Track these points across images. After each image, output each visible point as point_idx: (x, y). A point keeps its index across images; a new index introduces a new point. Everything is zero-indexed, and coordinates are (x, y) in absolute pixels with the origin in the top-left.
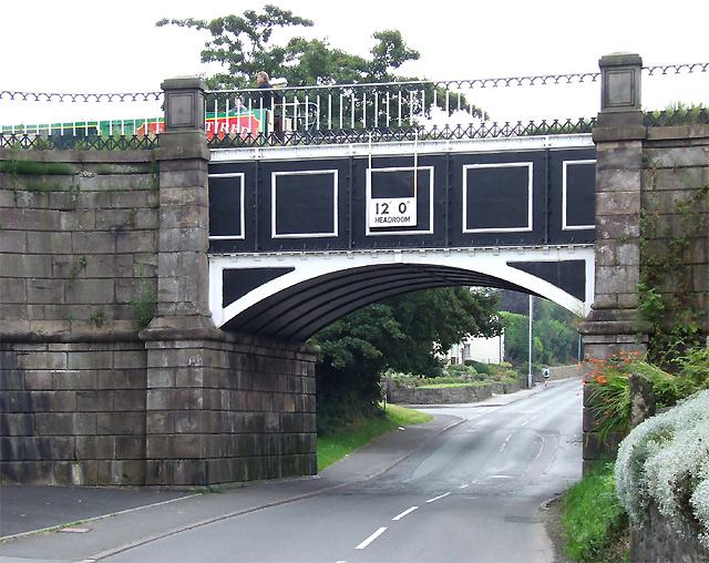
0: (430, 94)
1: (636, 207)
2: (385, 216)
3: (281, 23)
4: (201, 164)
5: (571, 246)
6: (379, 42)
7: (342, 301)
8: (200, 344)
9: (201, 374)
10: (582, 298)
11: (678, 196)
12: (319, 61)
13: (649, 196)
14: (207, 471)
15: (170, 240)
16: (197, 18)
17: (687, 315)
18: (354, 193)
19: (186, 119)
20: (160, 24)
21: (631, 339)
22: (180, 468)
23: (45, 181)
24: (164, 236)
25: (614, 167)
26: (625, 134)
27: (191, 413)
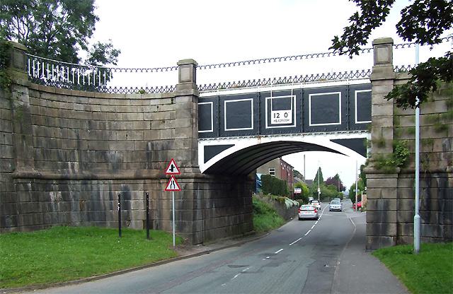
10: (206, 161)
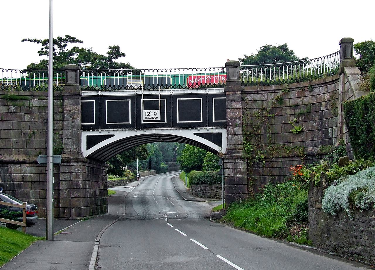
0: (128, 69)
1: (241, 114)
2: (148, 116)
3: (71, 41)
4: (79, 97)
5: (216, 128)
6: (110, 50)
7: (122, 148)
8: (81, 164)
9: (81, 175)
11: (254, 110)
12: (87, 56)
13: (244, 110)
14: (83, 212)
15: (68, 124)
16: (38, 39)
17: (259, 152)
18: (137, 108)
19: (73, 80)
20: (23, 41)
21: (241, 161)
22: (73, 211)
23: (19, 103)
24: (65, 123)
25: (232, 100)
26: (236, 89)
27: (78, 190)
